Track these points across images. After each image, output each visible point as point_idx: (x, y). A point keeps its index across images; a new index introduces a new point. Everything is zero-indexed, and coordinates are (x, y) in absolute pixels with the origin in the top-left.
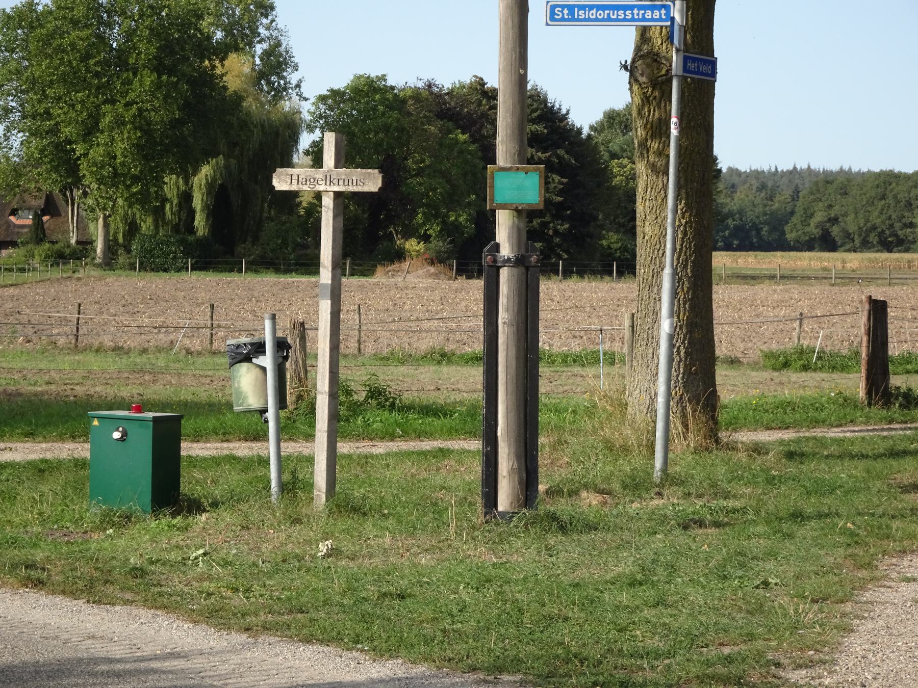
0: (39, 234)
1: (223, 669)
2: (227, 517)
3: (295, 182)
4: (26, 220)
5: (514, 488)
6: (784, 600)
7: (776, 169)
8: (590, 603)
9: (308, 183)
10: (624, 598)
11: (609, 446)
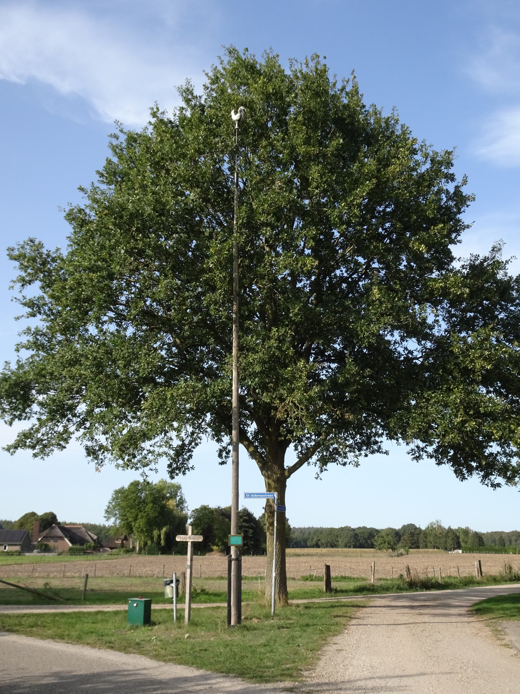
0: (122, 545)
1: (158, 673)
2: (162, 627)
4: (119, 542)
6: (303, 651)
8: (254, 652)
10: (262, 650)
11: (260, 605)
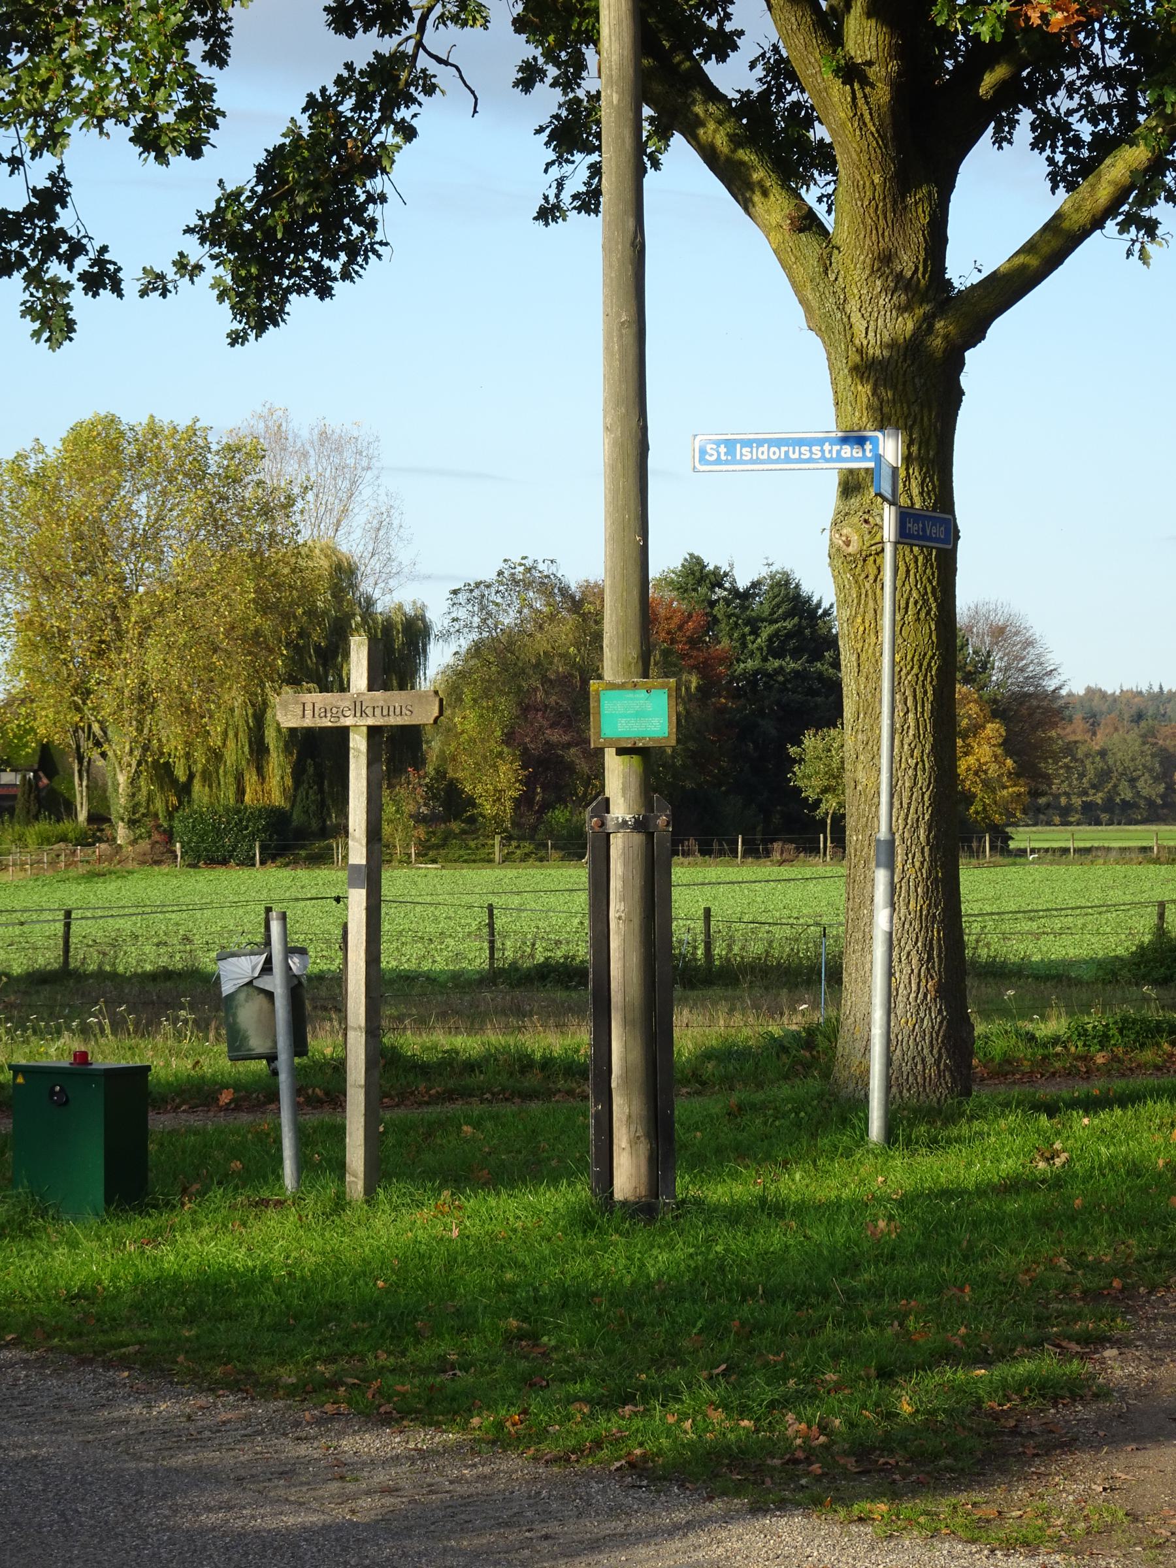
3: (308, 713)
5: (638, 1167)
7: (1161, 688)
9: (329, 715)
